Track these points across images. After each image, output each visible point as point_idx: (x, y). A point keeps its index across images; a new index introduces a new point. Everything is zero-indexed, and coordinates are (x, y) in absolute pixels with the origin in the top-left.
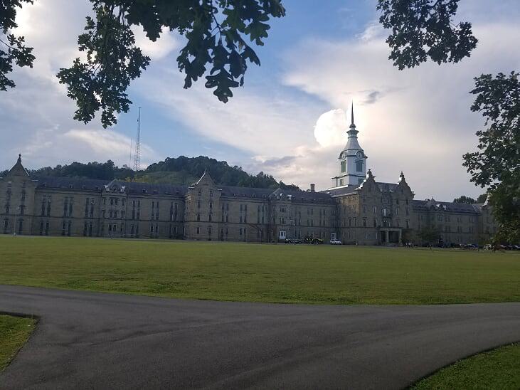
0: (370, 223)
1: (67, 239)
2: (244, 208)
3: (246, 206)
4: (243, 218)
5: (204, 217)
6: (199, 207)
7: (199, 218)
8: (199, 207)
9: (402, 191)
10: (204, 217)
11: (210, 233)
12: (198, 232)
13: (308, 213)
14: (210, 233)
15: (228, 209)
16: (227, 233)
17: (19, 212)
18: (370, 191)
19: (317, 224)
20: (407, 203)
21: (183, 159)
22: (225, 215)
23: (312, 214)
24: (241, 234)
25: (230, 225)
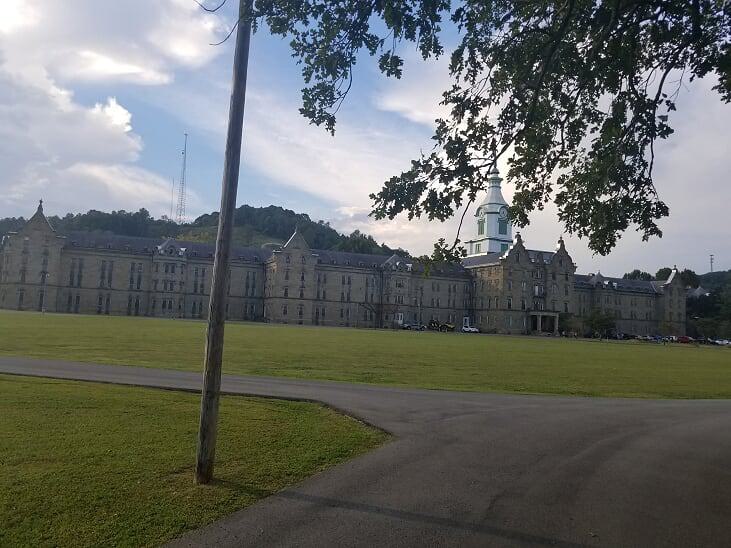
0: (516, 304)
5: (294, 293)
6: (287, 278)
7: (286, 294)
8: (287, 278)
10: (294, 293)
11: (301, 313)
19: (444, 304)
23: (438, 290)
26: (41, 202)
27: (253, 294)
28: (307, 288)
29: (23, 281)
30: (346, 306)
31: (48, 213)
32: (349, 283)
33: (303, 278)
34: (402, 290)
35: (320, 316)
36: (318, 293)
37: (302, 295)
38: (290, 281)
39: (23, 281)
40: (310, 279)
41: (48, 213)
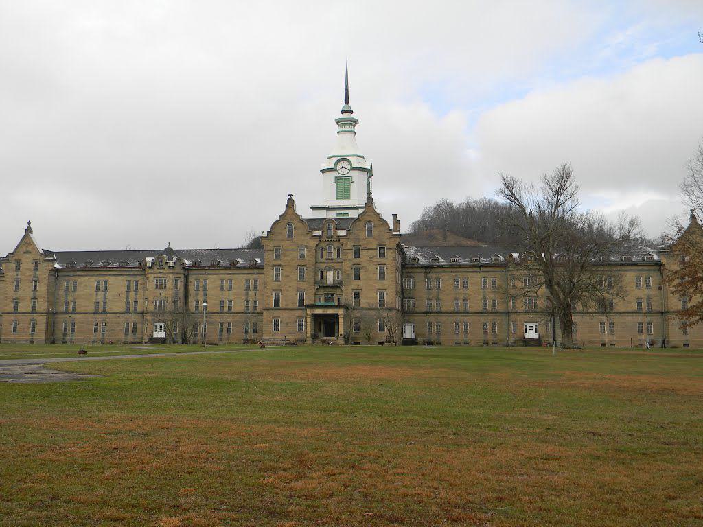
0: (289, 299)
1: (540, 348)
2: (102, 287)
3: (256, 281)
4: (101, 304)
5: (25, 306)
6: (17, 288)
7: (16, 308)
8: (17, 288)
9: (370, 231)
10: (25, 306)
11: (33, 330)
12: (15, 330)
13: (222, 287)
14: (33, 330)
15: (75, 290)
16: (73, 330)
17: (30, 309)
18: (290, 236)
19: (239, 306)
20: (382, 255)
21: (427, 226)
22: (251, 299)
23: (230, 287)
24: (96, 331)
25: (77, 317)
26: (29, 223)
27: (136, 309)
28: (39, 299)
29: (16, 311)
30: (100, 318)
31: (304, 211)
32: (106, 289)
33: (35, 287)
34: (163, 293)
35: (69, 332)
36: (247, 302)
37: (34, 308)
38: (20, 293)
39: (16, 311)
40: (42, 289)
41: (42, 242)
